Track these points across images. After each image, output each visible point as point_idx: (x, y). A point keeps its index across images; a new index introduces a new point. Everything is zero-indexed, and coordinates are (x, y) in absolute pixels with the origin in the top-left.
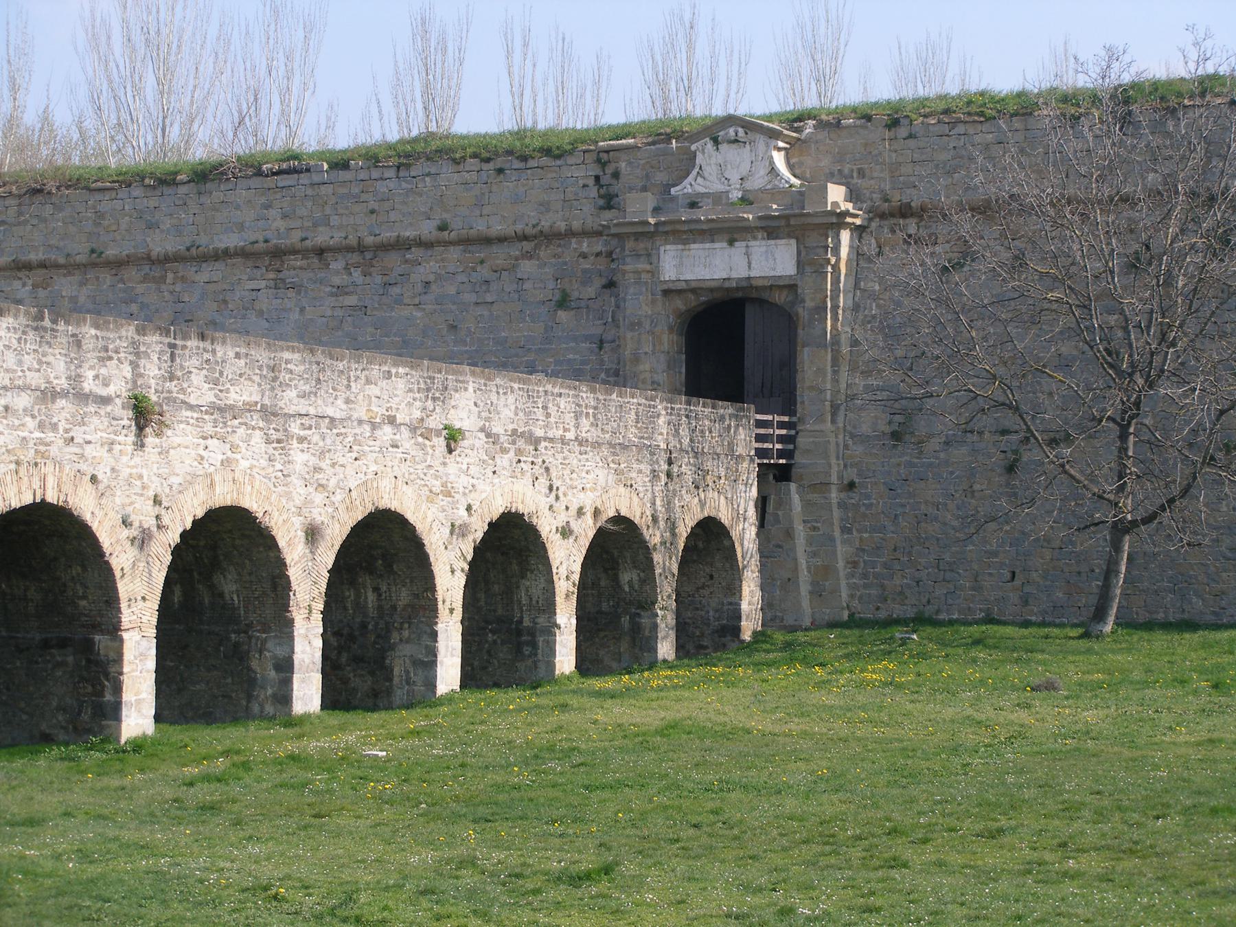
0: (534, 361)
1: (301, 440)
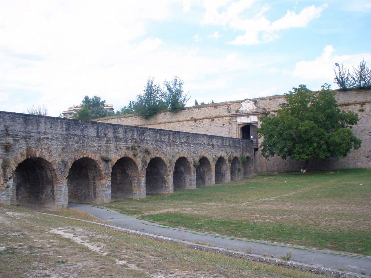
1: (192, 147)
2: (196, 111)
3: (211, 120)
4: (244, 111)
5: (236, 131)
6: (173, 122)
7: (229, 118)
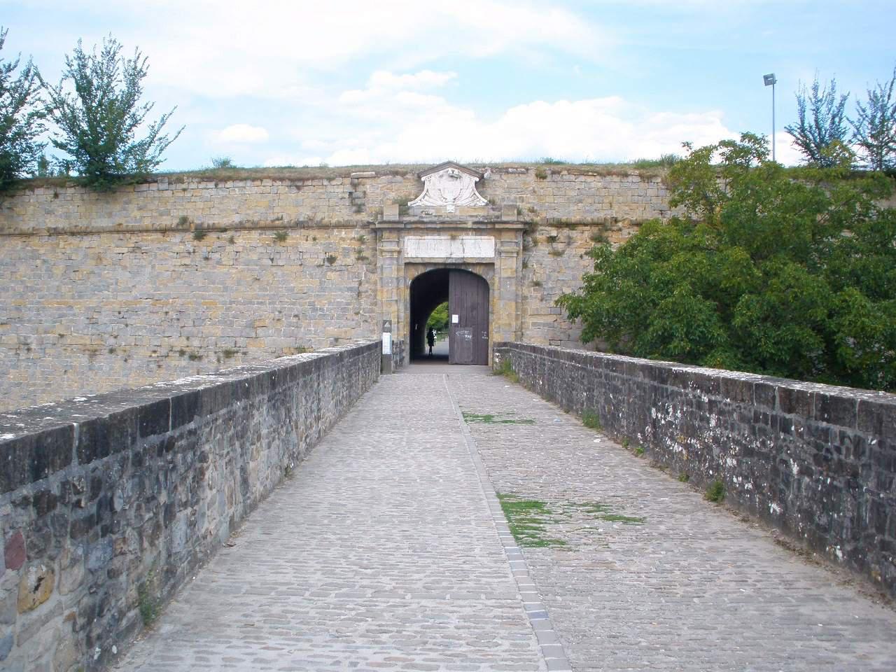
0: (314, 302)
2: (206, 194)
3: (272, 235)
4: (431, 211)
5: (395, 291)
6: (91, 233)
7: (354, 234)
